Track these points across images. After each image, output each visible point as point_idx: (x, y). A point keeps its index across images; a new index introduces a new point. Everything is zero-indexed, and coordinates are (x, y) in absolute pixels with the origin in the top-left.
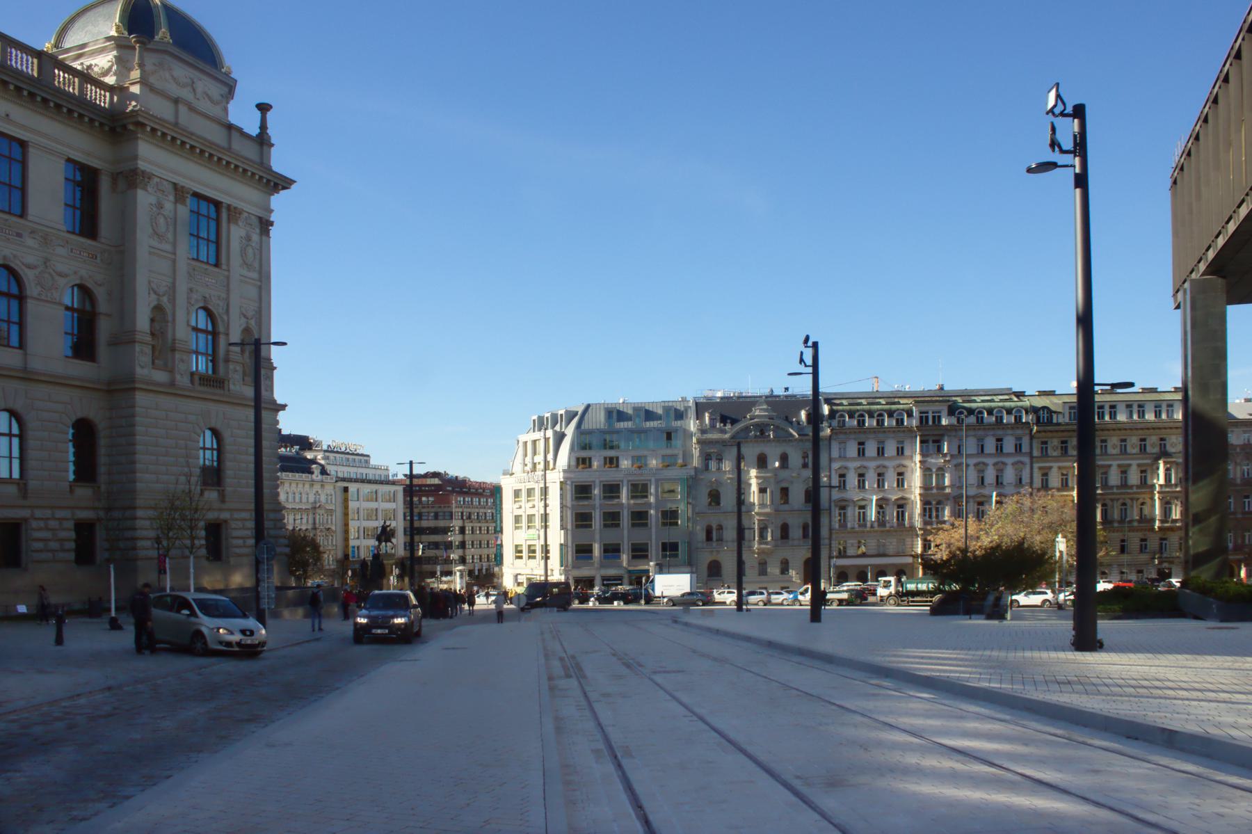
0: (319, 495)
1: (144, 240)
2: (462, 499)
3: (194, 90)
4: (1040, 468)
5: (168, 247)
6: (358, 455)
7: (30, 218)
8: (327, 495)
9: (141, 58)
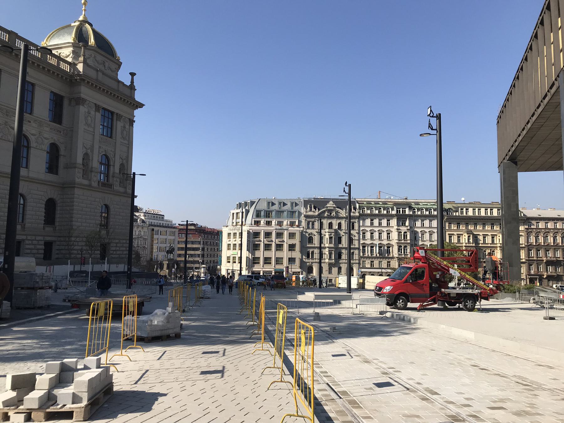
1: (82, 127)
3: (104, 66)
4: (449, 234)
5: (91, 129)
6: (159, 215)
7: (34, 115)
8: (144, 232)
9: (84, 52)
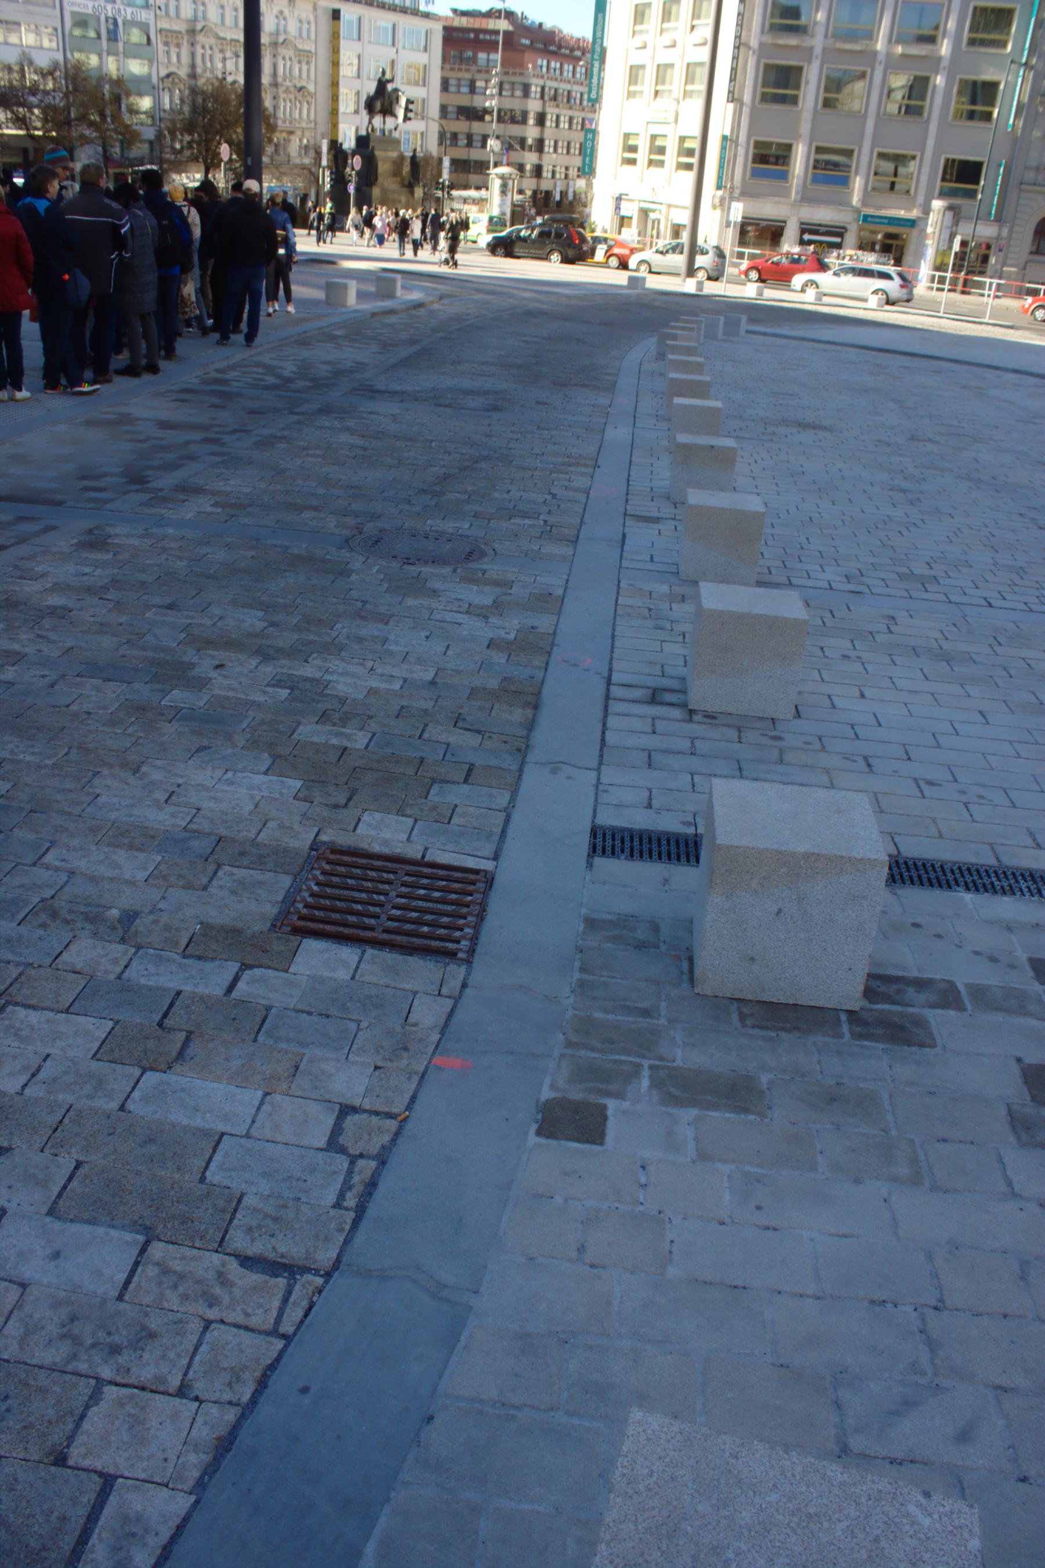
0: (285, 19)
2: (545, 63)
8: (301, 21)
